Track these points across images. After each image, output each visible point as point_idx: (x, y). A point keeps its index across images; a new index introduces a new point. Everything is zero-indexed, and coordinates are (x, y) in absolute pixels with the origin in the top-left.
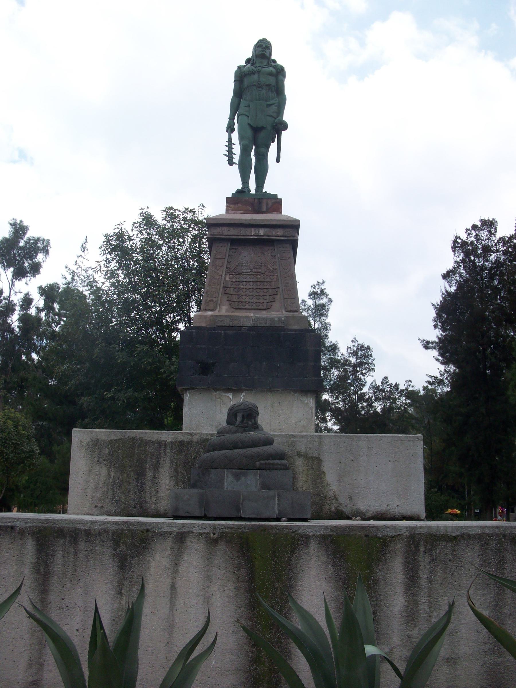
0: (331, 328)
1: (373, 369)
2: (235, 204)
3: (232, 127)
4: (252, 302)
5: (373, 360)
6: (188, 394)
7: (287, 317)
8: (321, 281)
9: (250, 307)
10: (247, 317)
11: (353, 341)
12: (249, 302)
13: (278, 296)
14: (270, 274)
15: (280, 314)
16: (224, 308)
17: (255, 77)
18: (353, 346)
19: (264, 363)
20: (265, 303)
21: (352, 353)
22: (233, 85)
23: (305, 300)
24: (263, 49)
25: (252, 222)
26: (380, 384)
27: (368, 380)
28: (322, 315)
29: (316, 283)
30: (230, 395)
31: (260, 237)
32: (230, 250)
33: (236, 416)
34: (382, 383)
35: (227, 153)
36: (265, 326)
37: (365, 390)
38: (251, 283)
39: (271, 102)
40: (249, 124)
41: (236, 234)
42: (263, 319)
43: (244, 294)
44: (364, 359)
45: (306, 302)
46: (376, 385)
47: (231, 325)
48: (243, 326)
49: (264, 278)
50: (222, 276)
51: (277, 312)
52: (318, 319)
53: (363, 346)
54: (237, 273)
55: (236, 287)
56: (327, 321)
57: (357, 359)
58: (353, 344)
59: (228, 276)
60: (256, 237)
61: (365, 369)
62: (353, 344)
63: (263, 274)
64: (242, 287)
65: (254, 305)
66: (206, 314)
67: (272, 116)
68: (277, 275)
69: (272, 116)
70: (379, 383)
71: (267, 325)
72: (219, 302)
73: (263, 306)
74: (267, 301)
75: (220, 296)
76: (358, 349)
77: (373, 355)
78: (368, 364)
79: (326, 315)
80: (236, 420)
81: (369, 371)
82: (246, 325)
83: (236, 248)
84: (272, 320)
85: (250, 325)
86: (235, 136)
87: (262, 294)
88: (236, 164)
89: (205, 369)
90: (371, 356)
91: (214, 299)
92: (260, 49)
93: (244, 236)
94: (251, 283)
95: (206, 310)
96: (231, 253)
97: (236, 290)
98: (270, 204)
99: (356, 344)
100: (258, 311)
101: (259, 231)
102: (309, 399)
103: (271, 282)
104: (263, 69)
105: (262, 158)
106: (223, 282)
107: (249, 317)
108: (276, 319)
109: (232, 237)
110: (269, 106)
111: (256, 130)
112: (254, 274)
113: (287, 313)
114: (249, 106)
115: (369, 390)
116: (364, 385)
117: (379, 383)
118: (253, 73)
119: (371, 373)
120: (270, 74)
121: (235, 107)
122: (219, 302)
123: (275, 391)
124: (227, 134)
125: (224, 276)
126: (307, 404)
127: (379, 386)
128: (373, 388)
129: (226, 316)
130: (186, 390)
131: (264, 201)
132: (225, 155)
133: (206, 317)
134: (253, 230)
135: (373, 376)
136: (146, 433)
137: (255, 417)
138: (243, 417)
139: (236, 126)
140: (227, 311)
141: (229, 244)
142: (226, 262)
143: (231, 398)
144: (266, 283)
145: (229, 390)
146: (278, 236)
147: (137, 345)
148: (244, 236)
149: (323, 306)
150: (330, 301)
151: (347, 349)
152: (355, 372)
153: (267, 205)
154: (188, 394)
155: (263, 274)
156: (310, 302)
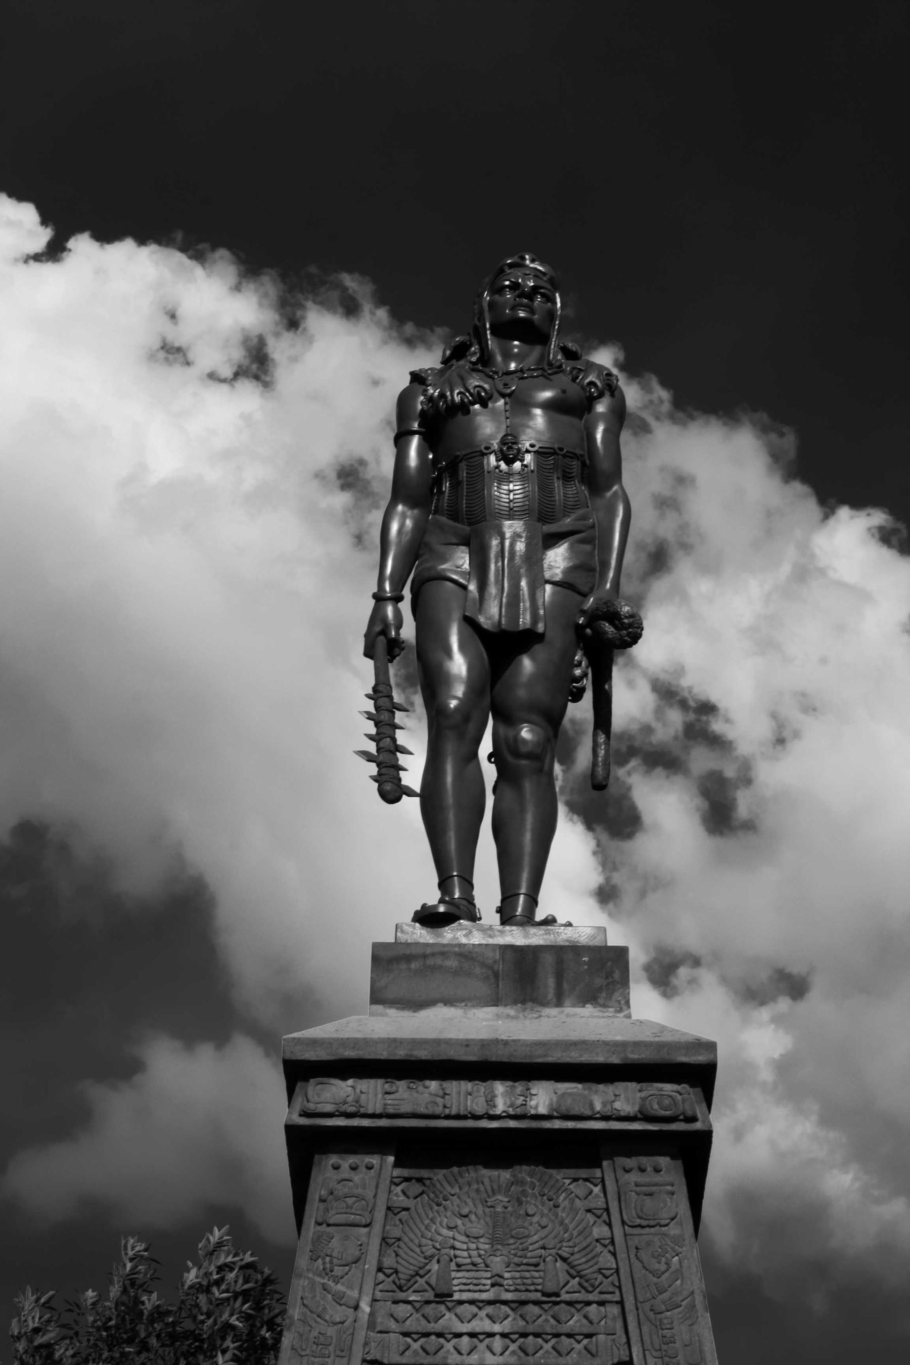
88: (410, 793)
93: (458, 1117)
132: (369, 757)
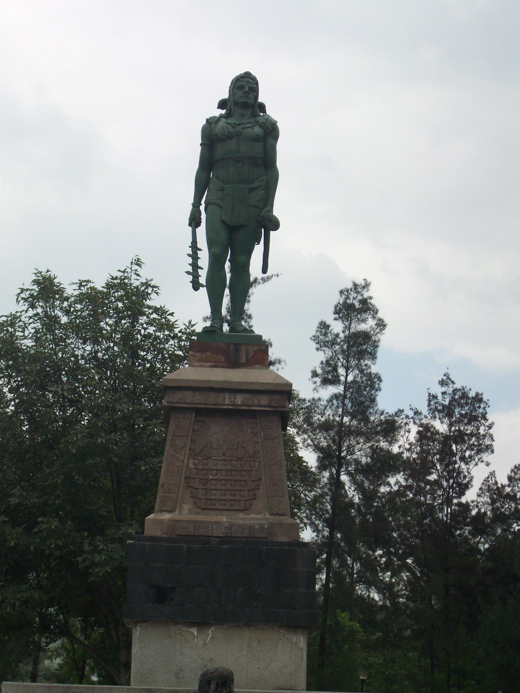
0: (382, 385)
1: (489, 449)
2: (202, 351)
3: (198, 220)
4: (224, 500)
5: (490, 427)
6: (139, 629)
7: (272, 525)
8: (360, 282)
9: (221, 507)
10: (218, 523)
11: (442, 383)
12: (221, 500)
13: (261, 491)
14: (249, 459)
15: (261, 519)
16: (186, 507)
17: (232, 144)
18: (444, 393)
19: (240, 589)
20: (242, 502)
21: (439, 411)
22: (200, 148)
23: (328, 323)
24: (244, 94)
25: (226, 386)
26: (506, 482)
27: (478, 474)
28: (361, 355)
29: (350, 286)
30: (194, 631)
31: (236, 408)
32: (195, 422)
33: (209, 683)
34: (510, 478)
35: (190, 269)
36: (242, 536)
37: (470, 496)
38: (224, 473)
39: (256, 184)
40: (223, 221)
41: (204, 402)
42: (240, 526)
43: (214, 487)
44: (469, 423)
45: (329, 326)
46: (496, 483)
47: (196, 534)
48: (212, 536)
49: (241, 465)
50: (183, 462)
51: (258, 514)
52: (353, 363)
53: (464, 396)
54: (205, 458)
55: (203, 477)
56: (374, 369)
57: (451, 425)
58: (444, 389)
59: (191, 461)
60: (231, 407)
61: (471, 447)
62: (444, 389)
63: (240, 459)
64: (211, 477)
65: (228, 504)
66: (162, 518)
67: (256, 207)
68: (260, 461)
69: (256, 207)
70: (502, 479)
71: (245, 535)
72: (179, 500)
73: (240, 505)
74: (245, 498)
75: (181, 491)
76: (453, 400)
77: (488, 416)
78: (477, 435)
79: (373, 356)
80: (210, 688)
81: (479, 451)
82: (215, 535)
83: (204, 419)
84: (251, 528)
85: (221, 535)
86: (202, 231)
87: (239, 488)
88: (203, 286)
89: (162, 595)
90: (484, 418)
91: (173, 496)
92: (240, 93)
93: (214, 404)
94: (224, 473)
95: (161, 511)
96: (196, 427)
97: (202, 481)
98: (251, 355)
99: (450, 390)
100: (233, 512)
101: (235, 398)
102: (298, 636)
103: (251, 471)
104: (246, 131)
105: (241, 269)
106: (184, 471)
107: (220, 521)
108: (257, 527)
109: (197, 406)
110: (252, 190)
111: (232, 229)
112: (227, 459)
113: (272, 517)
114: (222, 190)
115: (479, 496)
116: (467, 486)
117: (502, 479)
118: (228, 137)
119: (486, 457)
120: (256, 139)
121: (202, 184)
122: (179, 500)
123: (254, 625)
124: (190, 228)
125: (186, 462)
126: (296, 643)
127: (503, 486)
128: (489, 490)
129: (190, 522)
130: (136, 623)
131: (244, 348)
132: (188, 273)
133: (161, 522)
134: (227, 395)
135: (488, 464)
136: (94, 688)
137: (230, 684)
138: (217, 685)
139: (203, 216)
140: (190, 512)
141: (194, 415)
142: (189, 441)
143: (196, 634)
144: (243, 473)
145: (193, 624)
146: (262, 406)
147: (39, 519)
148: (214, 404)
149: (366, 336)
150: (381, 325)
151: (430, 401)
152: (446, 455)
153: (247, 353)
154: (139, 629)
155: (240, 459)
156: (327, 392)
